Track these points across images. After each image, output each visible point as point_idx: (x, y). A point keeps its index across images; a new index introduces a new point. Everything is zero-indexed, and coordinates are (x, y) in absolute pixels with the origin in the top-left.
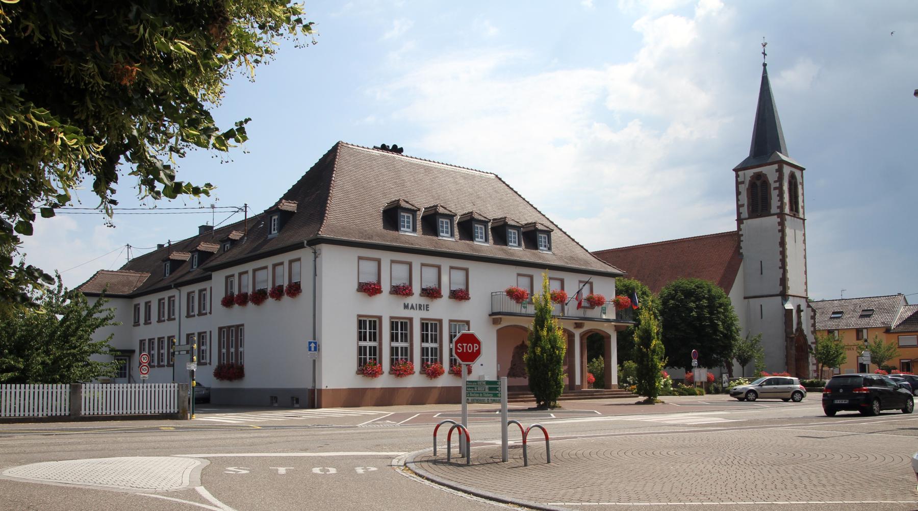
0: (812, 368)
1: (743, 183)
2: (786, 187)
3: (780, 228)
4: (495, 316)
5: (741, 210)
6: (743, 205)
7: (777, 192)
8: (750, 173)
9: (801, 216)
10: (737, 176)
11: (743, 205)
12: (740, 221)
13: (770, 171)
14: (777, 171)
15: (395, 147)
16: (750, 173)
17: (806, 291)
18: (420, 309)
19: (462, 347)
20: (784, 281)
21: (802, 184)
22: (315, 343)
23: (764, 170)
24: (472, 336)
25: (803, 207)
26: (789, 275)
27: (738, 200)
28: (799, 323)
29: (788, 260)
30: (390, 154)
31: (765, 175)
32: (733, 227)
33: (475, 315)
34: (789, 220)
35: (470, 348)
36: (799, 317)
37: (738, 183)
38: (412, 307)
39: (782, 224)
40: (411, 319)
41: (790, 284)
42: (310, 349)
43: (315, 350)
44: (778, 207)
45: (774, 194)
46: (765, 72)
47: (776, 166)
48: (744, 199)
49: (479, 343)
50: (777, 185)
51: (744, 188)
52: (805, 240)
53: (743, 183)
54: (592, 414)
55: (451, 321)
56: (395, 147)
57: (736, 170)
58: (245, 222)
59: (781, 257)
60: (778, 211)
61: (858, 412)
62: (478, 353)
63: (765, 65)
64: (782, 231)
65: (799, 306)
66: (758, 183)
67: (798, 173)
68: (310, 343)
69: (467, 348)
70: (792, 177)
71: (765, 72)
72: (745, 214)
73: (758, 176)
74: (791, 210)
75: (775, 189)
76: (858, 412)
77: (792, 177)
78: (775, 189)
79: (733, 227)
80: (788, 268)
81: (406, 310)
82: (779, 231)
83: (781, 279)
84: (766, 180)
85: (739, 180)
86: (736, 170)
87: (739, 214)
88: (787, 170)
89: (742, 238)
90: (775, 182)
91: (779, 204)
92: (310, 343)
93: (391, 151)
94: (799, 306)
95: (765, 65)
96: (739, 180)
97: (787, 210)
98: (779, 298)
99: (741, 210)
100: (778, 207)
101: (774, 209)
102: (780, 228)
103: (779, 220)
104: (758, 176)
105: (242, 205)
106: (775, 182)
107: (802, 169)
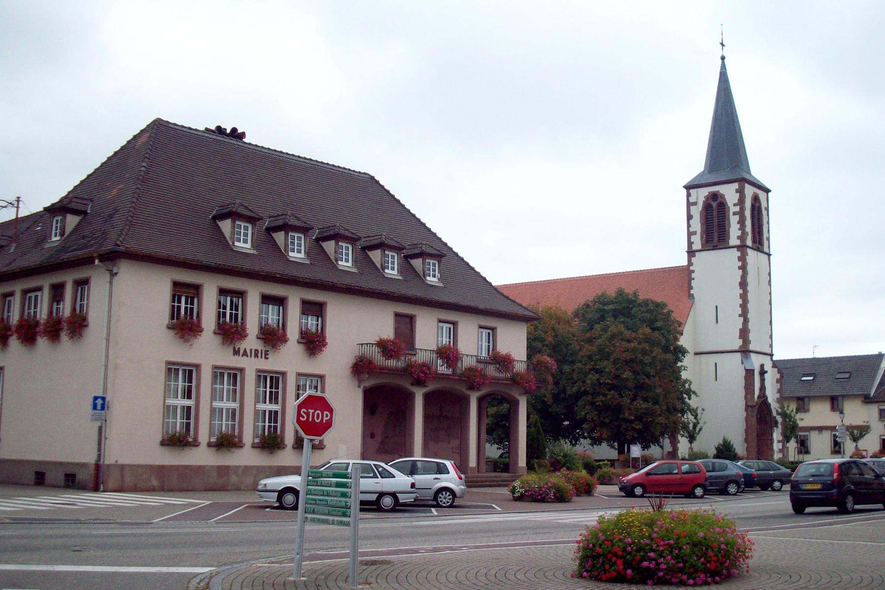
0: (777, 446)
1: (695, 204)
2: (748, 213)
3: (740, 264)
4: (361, 367)
5: (693, 238)
6: (695, 233)
7: (737, 218)
8: (704, 192)
9: (766, 250)
10: (689, 195)
11: (695, 233)
12: (691, 253)
13: (729, 193)
14: (737, 191)
15: (234, 130)
16: (704, 192)
17: (771, 346)
18: (256, 356)
19: (308, 414)
20: (744, 333)
21: (767, 209)
22: (103, 399)
23: (721, 189)
24: (322, 400)
25: (768, 239)
26: (750, 326)
27: (689, 226)
28: (763, 388)
29: (749, 306)
30: (227, 140)
31: (722, 196)
32: (685, 262)
33: (335, 364)
34: (752, 255)
35: (318, 416)
36: (763, 380)
37: (689, 205)
38: (245, 354)
39: (743, 259)
40: (242, 370)
41: (751, 337)
42: (95, 407)
43: (103, 408)
44: (738, 238)
45: (734, 220)
46: (723, 66)
47: (736, 186)
48: (697, 226)
49: (331, 410)
50: (737, 209)
51: (696, 211)
52: (770, 281)
53: (695, 204)
54: (488, 510)
55: (299, 375)
56: (234, 130)
57: (688, 187)
58: (17, 221)
59: (741, 302)
60: (738, 243)
61: (835, 508)
62: (328, 425)
63: (723, 58)
64: (743, 268)
65: (762, 366)
66: (714, 204)
67: (762, 195)
68: (96, 398)
69: (315, 420)
70: (756, 199)
71: (723, 66)
72: (697, 245)
73: (715, 196)
74: (754, 241)
75: (735, 214)
76: (835, 508)
77: (756, 199)
78: (735, 214)
79: (685, 262)
80: (749, 316)
81: (236, 357)
82: (739, 268)
83: (741, 330)
84: (728, 208)
85: (692, 200)
86: (688, 187)
87: (690, 244)
88: (749, 191)
89: (693, 275)
90: (735, 205)
91: (739, 233)
92: (96, 398)
93: (228, 135)
94: (762, 366)
95: (723, 58)
96: (155, 483)
97: (749, 242)
98: (739, 355)
99: (693, 238)
100: (738, 238)
101: (734, 241)
102: (740, 264)
103: (739, 254)
104: (715, 196)
105: (12, 199)
106: (735, 205)
107: (767, 191)
